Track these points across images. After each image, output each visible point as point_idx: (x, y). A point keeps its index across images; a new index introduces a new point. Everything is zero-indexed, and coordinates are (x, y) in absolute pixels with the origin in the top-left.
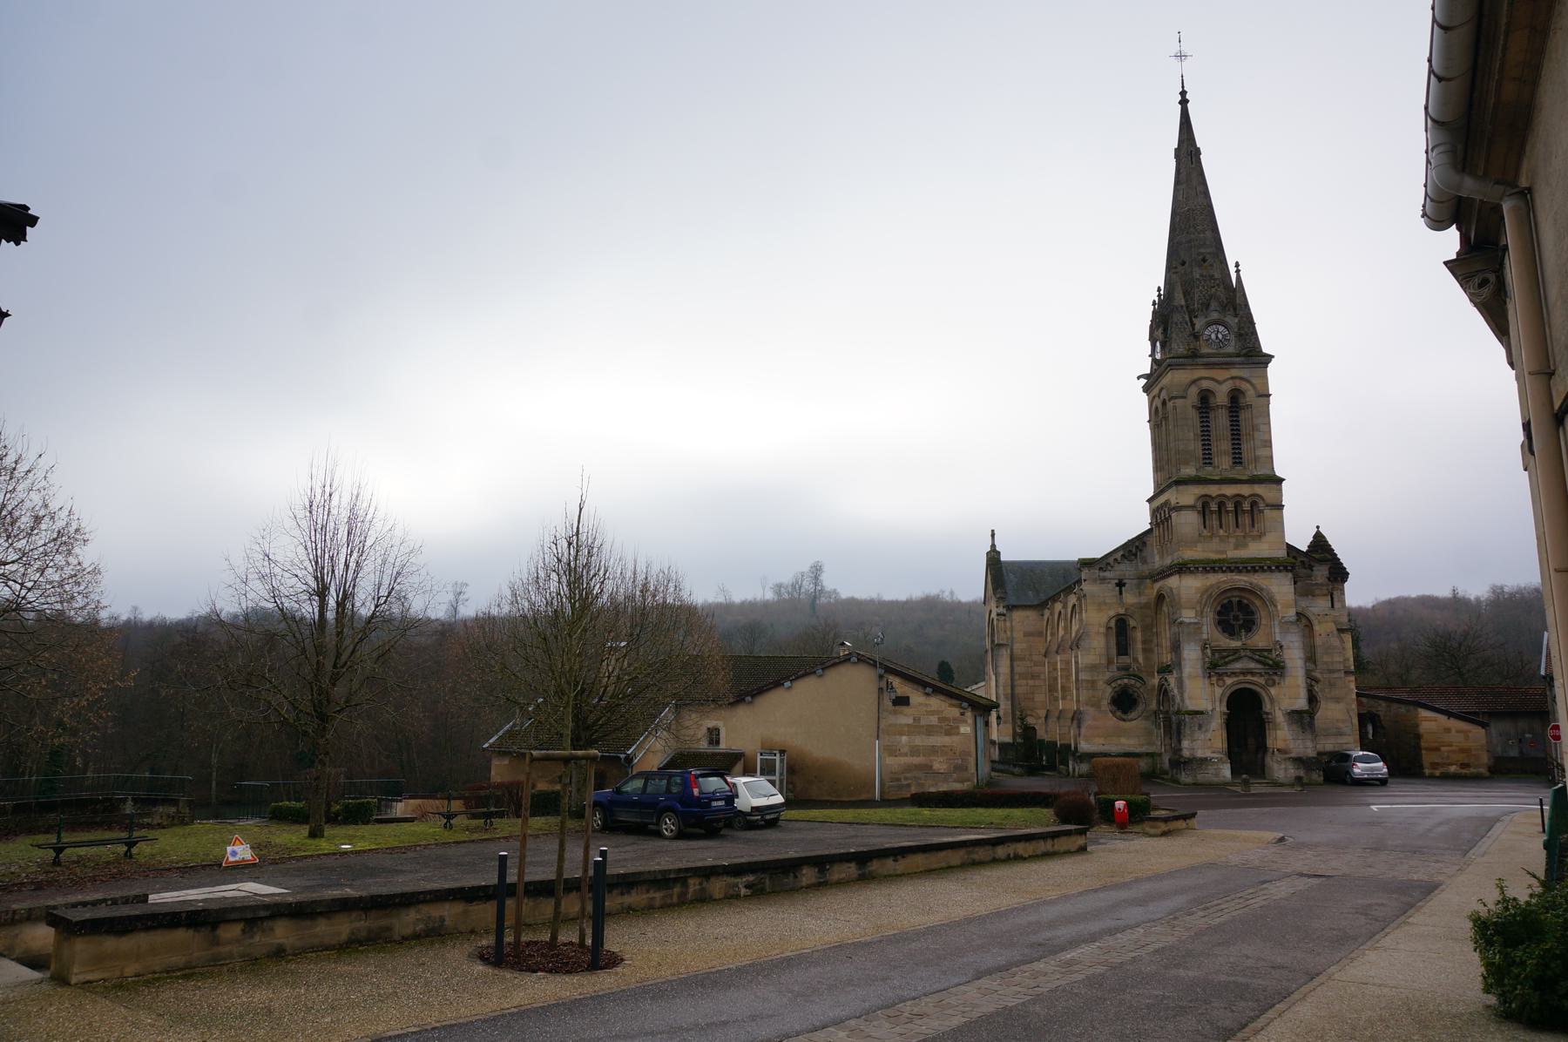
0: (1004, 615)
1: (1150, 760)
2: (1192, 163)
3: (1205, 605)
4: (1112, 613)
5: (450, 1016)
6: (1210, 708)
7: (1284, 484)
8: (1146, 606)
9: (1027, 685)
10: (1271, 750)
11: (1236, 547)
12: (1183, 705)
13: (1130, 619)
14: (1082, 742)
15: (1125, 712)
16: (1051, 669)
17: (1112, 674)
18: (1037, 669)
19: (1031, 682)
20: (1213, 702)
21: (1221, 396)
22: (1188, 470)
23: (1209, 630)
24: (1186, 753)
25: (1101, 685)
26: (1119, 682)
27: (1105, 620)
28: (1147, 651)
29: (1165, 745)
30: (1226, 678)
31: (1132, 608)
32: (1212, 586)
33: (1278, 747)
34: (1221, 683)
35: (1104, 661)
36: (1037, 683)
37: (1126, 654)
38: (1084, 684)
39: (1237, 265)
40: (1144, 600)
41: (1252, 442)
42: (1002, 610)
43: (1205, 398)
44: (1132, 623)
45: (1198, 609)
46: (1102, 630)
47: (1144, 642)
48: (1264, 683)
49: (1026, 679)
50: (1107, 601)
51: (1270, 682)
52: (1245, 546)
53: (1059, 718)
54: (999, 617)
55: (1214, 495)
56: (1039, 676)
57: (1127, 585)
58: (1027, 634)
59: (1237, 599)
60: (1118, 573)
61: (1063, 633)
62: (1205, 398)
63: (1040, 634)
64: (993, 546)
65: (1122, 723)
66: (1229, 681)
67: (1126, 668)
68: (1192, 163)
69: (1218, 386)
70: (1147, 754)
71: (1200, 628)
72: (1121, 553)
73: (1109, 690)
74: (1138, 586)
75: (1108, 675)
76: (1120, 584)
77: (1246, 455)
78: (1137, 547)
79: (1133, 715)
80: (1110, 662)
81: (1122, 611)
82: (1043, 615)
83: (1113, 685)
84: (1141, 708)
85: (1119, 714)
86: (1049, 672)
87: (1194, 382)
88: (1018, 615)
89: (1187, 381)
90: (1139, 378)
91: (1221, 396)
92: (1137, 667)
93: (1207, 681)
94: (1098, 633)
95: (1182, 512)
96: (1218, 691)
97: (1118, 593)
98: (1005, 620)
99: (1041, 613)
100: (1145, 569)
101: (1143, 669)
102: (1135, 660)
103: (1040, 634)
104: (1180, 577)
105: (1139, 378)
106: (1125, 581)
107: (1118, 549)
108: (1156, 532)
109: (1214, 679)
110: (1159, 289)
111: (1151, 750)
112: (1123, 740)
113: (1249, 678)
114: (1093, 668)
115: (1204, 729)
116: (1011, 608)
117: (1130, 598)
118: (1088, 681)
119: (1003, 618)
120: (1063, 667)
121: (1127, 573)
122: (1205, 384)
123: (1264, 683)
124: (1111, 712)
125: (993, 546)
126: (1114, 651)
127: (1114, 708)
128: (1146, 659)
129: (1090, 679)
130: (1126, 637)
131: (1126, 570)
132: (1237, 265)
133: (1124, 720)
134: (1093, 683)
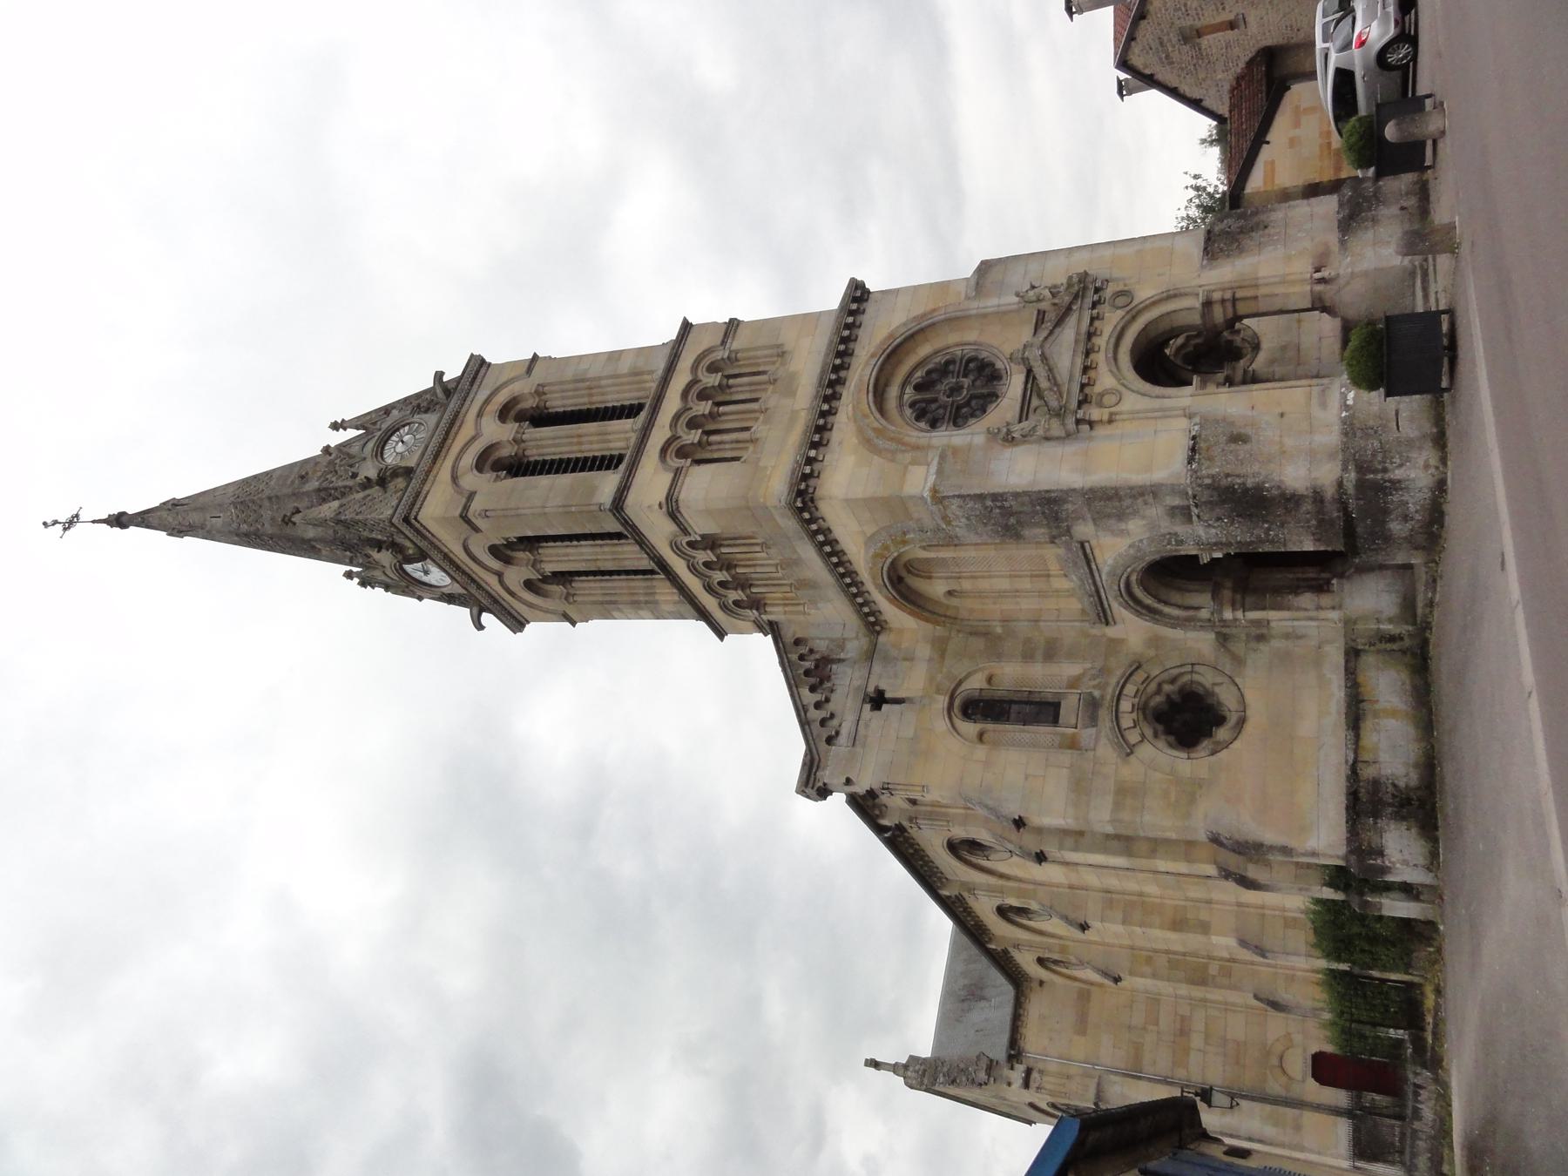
0: (1029, 1072)
1: (1369, 661)
2: (219, 517)
3: (900, 442)
4: (942, 725)
5: (1455, 1147)
6: (1183, 423)
7: (693, 320)
8: (940, 648)
9: (1205, 1053)
10: (1319, 288)
11: (791, 392)
12: (1175, 490)
13: (966, 686)
14: (1312, 843)
15: (1220, 720)
16: (1147, 970)
17: (1103, 741)
18: (1166, 1022)
19: (1197, 1041)
20: (1165, 414)
21: (496, 432)
22: (607, 490)
23: (972, 435)
24: (1327, 474)
25: (1132, 771)
26: (1126, 722)
27: (954, 743)
28: (1051, 653)
29: (1319, 608)
30: (1098, 389)
31: (939, 677)
32: (860, 431)
33: (1310, 269)
34: (1108, 400)
35: (1066, 757)
36: (1198, 1024)
37: (1056, 706)
38: (1125, 815)
39: (335, 426)
40: (924, 651)
41: (603, 382)
42: (1017, 1075)
43: (489, 461)
44: (976, 683)
45: (908, 456)
46: (981, 752)
47: (1028, 657)
48: (1120, 313)
49: (1187, 1051)
50: (910, 733)
51: (1121, 301)
52: (792, 377)
53: (1261, 951)
54: (1033, 1085)
55: (668, 434)
56: (1183, 1018)
57: (882, 687)
58: (1082, 1025)
59: (909, 390)
60: (849, 703)
61: (1055, 920)
62: (489, 461)
63: (1084, 997)
64: (895, 1068)
65: (1249, 728)
66: (1105, 380)
67: (1093, 705)
68: (219, 517)
69: (481, 439)
70: (1351, 673)
71: (955, 451)
72: (805, 692)
73: (1147, 751)
74: (887, 659)
75: (1106, 752)
76: (878, 700)
77: (626, 398)
78: (802, 658)
79: (1226, 698)
80: (1072, 744)
81: (942, 701)
82: (1041, 983)
83: (1133, 737)
84: (1206, 678)
85: (1222, 733)
86: (1154, 976)
87: (455, 479)
88: (1033, 1041)
89: (450, 488)
90: (480, 627)
91: (496, 432)
92: (1094, 677)
93: (1100, 431)
94: (987, 764)
95: (682, 497)
96: (1131, 402)
97: (896, 707)
98: (1041, 1072)
99: (1035, 985)
100: (855, 646)
101: (1098, 665)
102: (1074, 683)
103: (1084, 997)
104: (820, 499)
105: (480, 627)
106: (871, 689)
107: (792, 696)
108: (775, 614)
109: (1095, 413)
110: (349, 575)
111: (1335, 655)
112: (1306, 728)
113: (1101, 342)
114: (1080, 787)
115: (1249, 431)
116: (1015, 1053)
117: (911, 681)
118: (1117, 806)
119: (1035, 1075)
120: (1120, 916)
121: (856, 683)
122: (469, 459)
123: (1120, 313)
124: (1213, 753)
125: (895, 1068)
126: (1043, 732)
127: (1206, 744)
128: (1072, 655)
129: (1110, 799)
130: (1011, 702)
131: (848, 682)
132: (335, 426)
133: (1242, 722)
134: (1124, 792)
